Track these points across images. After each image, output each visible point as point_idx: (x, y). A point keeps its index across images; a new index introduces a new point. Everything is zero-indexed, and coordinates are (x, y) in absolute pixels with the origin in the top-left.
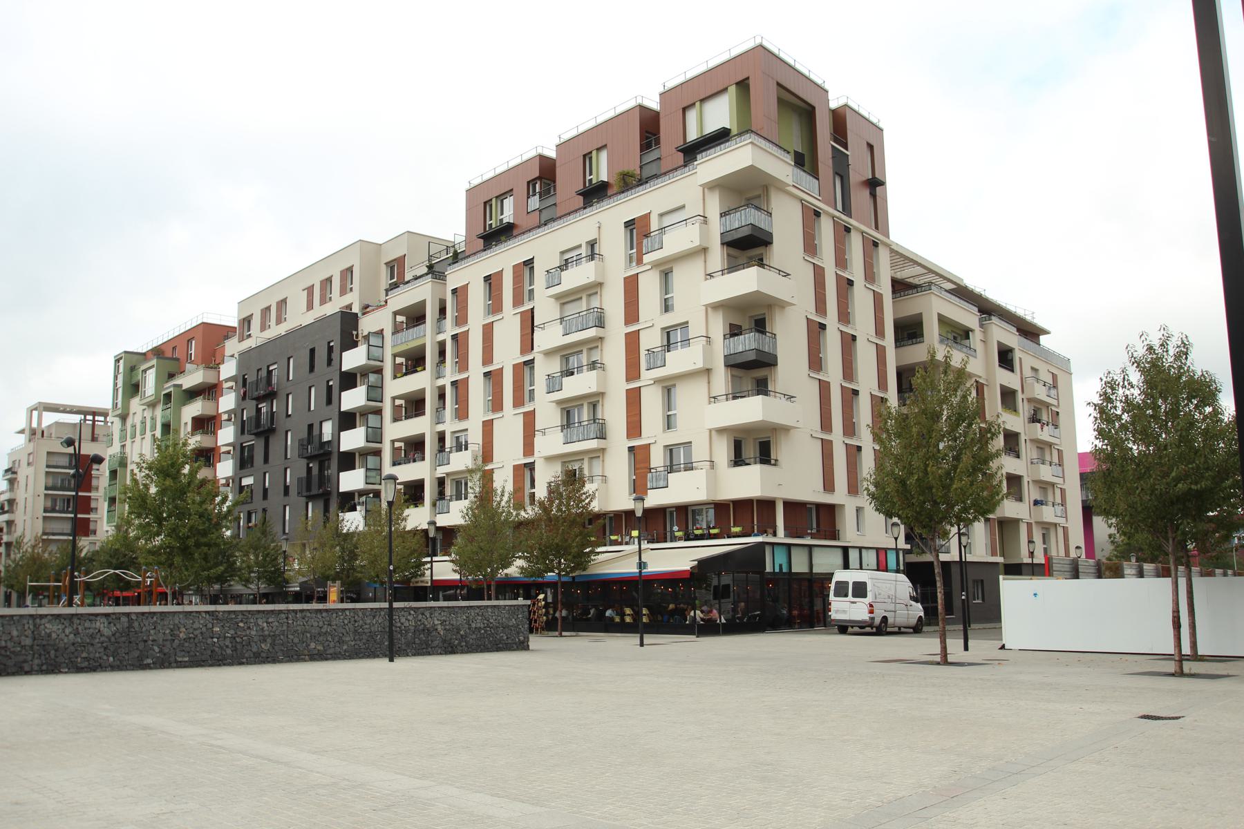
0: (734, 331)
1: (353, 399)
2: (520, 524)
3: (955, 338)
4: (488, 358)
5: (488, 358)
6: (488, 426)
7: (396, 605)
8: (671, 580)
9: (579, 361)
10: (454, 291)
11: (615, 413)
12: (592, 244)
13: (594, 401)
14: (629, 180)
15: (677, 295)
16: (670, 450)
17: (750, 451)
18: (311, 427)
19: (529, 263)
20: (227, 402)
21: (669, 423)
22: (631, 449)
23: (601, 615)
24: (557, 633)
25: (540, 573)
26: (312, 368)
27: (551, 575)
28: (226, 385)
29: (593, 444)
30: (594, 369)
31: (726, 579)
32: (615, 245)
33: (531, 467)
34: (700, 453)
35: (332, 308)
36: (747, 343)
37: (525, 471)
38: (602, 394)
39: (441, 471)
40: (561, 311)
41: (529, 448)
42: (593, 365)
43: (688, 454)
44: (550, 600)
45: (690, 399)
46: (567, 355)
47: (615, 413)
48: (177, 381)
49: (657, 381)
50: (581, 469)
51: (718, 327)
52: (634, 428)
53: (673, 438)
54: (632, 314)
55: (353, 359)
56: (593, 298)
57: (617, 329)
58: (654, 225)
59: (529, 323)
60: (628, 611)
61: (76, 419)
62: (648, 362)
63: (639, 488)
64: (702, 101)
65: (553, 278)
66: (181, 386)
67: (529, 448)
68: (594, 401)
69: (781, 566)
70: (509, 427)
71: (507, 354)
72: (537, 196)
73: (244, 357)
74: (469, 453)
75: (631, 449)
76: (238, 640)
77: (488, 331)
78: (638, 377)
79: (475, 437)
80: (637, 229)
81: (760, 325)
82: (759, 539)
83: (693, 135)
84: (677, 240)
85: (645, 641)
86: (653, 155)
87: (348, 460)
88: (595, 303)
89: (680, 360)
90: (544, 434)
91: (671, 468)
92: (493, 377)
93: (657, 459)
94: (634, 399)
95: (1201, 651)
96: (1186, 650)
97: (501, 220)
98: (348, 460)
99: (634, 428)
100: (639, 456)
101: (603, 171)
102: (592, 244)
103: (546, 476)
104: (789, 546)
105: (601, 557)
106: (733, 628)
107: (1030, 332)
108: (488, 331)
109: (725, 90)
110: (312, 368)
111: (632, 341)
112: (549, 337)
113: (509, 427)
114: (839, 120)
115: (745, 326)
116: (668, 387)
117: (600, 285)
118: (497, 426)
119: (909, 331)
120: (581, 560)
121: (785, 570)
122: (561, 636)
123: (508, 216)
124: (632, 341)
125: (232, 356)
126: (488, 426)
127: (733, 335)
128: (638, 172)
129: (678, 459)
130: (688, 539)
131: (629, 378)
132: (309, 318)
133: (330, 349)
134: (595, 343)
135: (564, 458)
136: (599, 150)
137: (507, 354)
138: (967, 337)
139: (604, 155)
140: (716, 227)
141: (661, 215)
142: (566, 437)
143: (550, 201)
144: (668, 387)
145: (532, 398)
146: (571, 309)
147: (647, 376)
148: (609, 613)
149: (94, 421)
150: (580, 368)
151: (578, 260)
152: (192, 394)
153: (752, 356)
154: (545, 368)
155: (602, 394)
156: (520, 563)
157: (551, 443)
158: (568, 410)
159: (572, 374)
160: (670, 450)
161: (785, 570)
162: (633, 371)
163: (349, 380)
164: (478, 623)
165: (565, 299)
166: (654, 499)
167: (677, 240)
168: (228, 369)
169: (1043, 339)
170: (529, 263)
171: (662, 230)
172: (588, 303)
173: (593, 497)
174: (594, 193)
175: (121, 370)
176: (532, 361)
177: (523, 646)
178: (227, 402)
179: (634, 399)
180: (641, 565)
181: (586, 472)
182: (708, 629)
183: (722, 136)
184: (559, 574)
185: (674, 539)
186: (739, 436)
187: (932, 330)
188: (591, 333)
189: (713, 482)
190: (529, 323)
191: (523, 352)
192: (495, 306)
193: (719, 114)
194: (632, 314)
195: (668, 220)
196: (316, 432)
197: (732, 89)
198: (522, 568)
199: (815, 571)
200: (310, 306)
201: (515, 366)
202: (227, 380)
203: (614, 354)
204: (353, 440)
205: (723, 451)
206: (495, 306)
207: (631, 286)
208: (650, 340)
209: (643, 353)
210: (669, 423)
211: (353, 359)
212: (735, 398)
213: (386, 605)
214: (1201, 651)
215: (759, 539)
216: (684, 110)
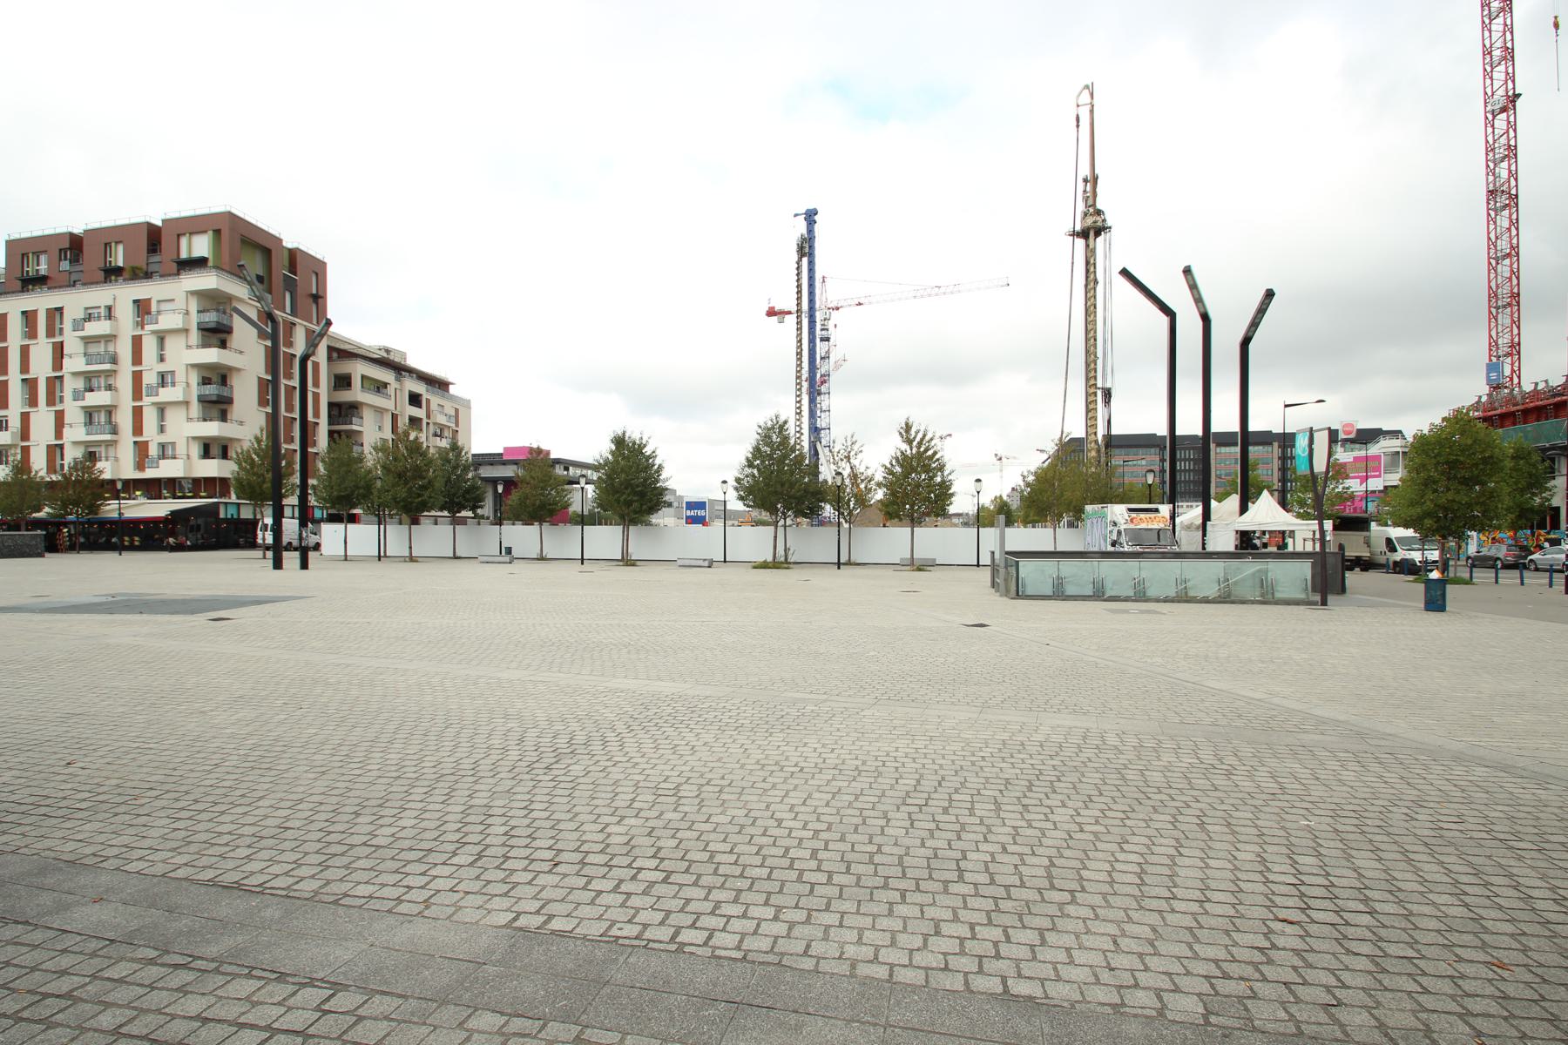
0: (206, 381)
2: (52, 485)
3: (378, 388)
4: (25, 367)
5: (25, 367)
6: (25, 417)
8: (155, 521)
9: (99, 383)
11: (124, 419)
12: (109, 308)
13: (110, 410)
14: (137, 271)
15: (168, 352)
16: (163, 446)
17: (215, 450)
19: (60, 310)
21: (162, 429)
22: (135, 442)
23: (108, 541)
25: (63, 516)
27: (71, 518)
29: (108, 437)
30: (110, 390)
31: (200, 521)
32: (125, 313)
33: (61, 447)
34: (181, 449)
36: (212, 390)
37: (55, 451)
38: (115, 407)
40: (86, 348)
41: (59, 434)
42: (109, 388)
43: (174, 449)
44: (73, 532)
45: (175, 419)
46: (90, 381)
47: (124, 419)
49: (154, 332)
50: (100, 452)
51: (194, 379)
52: (138, 429)
53: (163, 439)
54: (137, 358)
56: (109, 344)
57: (126, 368)
58: (154, 308)
59: (59, 352)
60: (126, 538)
62: (147, 392)
63: (140, 466)
64: (191, 234)
65: (78, 325)
67: (59, 434)
68: (110, 410)
70: (42, 421)
71: (41, 366)
72: (68, 262)
74: (8, 433)
75: (135, 442)
77: (25, 351)
78: (141, 399)
80: (142, 308)
81: (224, 380)
82: (215, 500)
83: (184, 255)
84: (168, 321)
85: (1525, 581)
86: (156, 258)
88: (111, 348)
89: (166, 395)
90: (71, 427)
91: (163, 456)
92: (30, 385)
93: (153, 451)
94: (138, 413)
95: (458, 554)
96: (382, 554)
97: (37, 270)
99: (138, 429)
100: (141, 449)
101: (119, 259)
102: (109, 308)
103: (72, 455)
104: (239, 504)
105: (108, 508)
106: (195, 548)
107: (440, 385)
108: (25, 351)
109: (205, 232)
111: (137, 377)
112: (75, 363)
113: (42, 421)
114: (294, 255)
115: (214, 379)
116: (162, 409)
117: (115, 336)
118: (33, 418)
119: (343, 382)
120: (94, 509)
123: (43, 268)
124: (137, 377)
126: (25, 417)
127: (204, 384)
128: (145, 267)
129: (165, 451)
130: (174, 498)
131: (135, 399)
134: (111, 373)
135: (87, 444)
136: (117, 243)
137: (41, 366)
138: (386, 387)
139: (121, 248)
140: (194, 318)
141: (159, 301)
142: (87, 430)
143: (78, 268)
144: (162, 409)
145: (62, 400)
146: (93, 349)
147: (147, 400)
148: (113, 540)
150: (99, 388)
151: (99, 318)
153: (214, 398)
154: (70, 385)
155: (115, 407)
156: (47, 509)
157: (75, 432)
158: (90, 413)
159: (92, 391)
160: (163, 446)
161: (235, 517)
162: (137, 395)
164: (10, 543)
165: (88, 341)
166: (150, 474)
167: (168, 321)
169: (452, 389)
170: (60, 310)
171: (159, 312)
172: (106, 346)
173: (101, 472)
174: (112, 274)
176: (62, 377)
177: (44, 556)
179: (138, 413)
180: (120, 514)
181: (103, 455)
182: (179, 548)
183: (199, 263)
184: (77, 517)
185: (165, 498)
186: (207, 442)
187: (356, 382)
188: (107, 367)
189: (188, 465)
190: (59, 352)
191: (54, 369)
192: (31, 332)
193: (201, 246)
194: (137, 358)
195: (164, 306)
197: (211, 233)
198: (48, 513)
199: (242, 517)
201: (48, 378)
203: (124, 382)
205: (196, 450)
206: (31, 332)
207: (137, 342)
208: (149, 378)
209: (144, 386)
210: (162, 429)
212: (205, 420)
214: (853, 560)
215: (215, 500)
216: (179, 236)
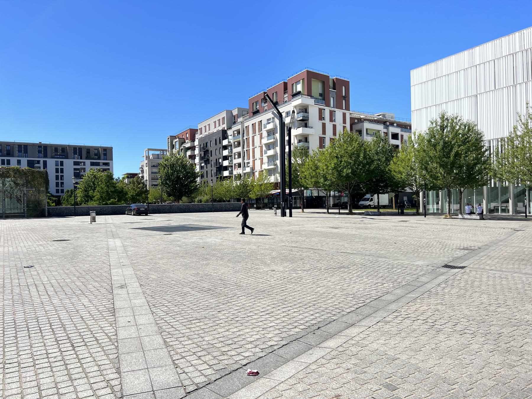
1: (226, 153)
7: (76, 206)
10: (246, 127)
18: (216, 159)
20: (197, 152)
24: (347, 211)
26: (216, 144)
28: (196, 147)
35: (220, 128)
39: (244, 172)
48: (184, 145)
55: (225, 142)
61: (158, 152)
66: (185, 146)
69: (309, 194)
73: (200, 140)
74: (249, 168)
76: (492, 308)
77: (253, 137)
79: (251, 165)
87: (226, 168)
98: (226, 168)
110: (216, 144)
121: (310, 195)
122: (351, 213)
125: (198, 139)
132: (215, 131)
133: (220, 140)
149: (163, 153)
152: (188, 149)
163: (225, 148)
168: (196, 143)
170: (261, 121)
175: (169, 141)
178: (197, 152)
196: (218, 161)
200: (215, 127)
202: (197, 146)
204: (226, 163)
211: (225, 142)
213: (74, 207)
